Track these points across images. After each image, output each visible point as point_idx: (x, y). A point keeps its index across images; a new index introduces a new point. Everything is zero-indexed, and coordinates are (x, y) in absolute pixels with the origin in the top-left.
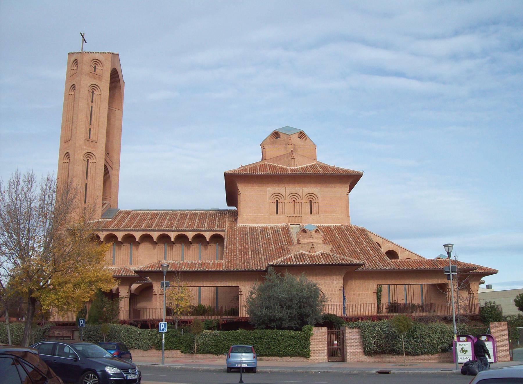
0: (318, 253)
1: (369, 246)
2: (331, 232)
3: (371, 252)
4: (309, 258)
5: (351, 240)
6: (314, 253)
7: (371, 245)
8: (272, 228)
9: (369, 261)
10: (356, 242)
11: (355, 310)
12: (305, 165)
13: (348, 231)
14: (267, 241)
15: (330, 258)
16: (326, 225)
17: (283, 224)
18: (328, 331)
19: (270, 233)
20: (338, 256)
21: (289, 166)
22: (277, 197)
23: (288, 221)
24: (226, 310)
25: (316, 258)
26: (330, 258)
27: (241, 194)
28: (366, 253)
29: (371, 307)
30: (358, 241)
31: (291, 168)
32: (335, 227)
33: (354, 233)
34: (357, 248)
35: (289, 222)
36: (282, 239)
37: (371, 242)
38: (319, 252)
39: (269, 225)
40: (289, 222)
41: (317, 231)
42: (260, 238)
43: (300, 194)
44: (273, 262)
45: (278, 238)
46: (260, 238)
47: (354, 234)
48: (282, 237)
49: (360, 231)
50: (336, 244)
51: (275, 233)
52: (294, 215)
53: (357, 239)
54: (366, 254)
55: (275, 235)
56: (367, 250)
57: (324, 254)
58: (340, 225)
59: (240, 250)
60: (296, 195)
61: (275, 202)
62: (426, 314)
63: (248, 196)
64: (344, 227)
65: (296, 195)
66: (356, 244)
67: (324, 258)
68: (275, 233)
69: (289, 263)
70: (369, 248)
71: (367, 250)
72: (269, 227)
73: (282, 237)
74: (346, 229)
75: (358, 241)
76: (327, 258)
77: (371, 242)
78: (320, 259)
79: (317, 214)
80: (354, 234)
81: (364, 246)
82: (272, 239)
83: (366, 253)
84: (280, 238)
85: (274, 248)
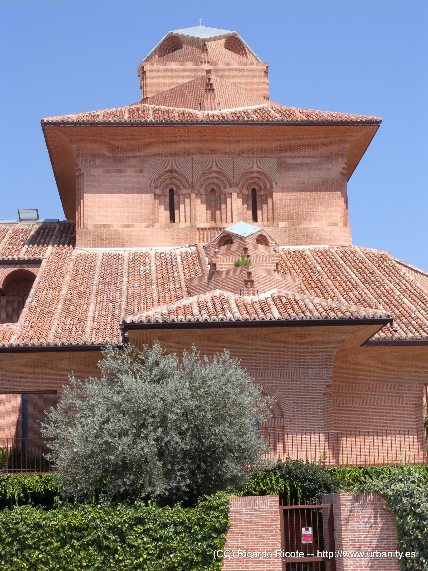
0: (262, 296)
1: (401, 289)
2: (303, 261)
3: (406, 301)
4: (238, 307)
5: (354, 276)
6: (254, 295)
7: (405, 288)
8: (158, 256)
9: (401, 320)
10: (367, 282)
11: (367, 451)
12: (241, 109)
13: (345, 259)
14: (142, 280)
15: (296, 306)
16: (292, 248)
17: (187, 245)
18: (289, 507)
19: (153, 264)
20: (317, 301)
21: (201, 106)
22: (172, 181)
23: (199, 240)
24: (337, 519)
25: (257, 306)
26: (296, 306)
27: (83, 174)
28: (393, 304)
29: (407, 444)
30: (372, 278)
31: (206, 112)
32: (313, 252)
33: (361, 263)
34: (368, 292)
35: (201, 241)
36: (179, 277)
37: (403, 281)
38: (268, 294)
39: (152, 251)
40: (201, 241)
41: (261, 239)
42: (125, 274)
43: (228, 172)
44: (138, 316)
45: (170, 274)
46: (125, 274)
47: (360, 265)
48: (181, 273)
49: (375, 258)
50: (315, 286)
51: (164, 265)
52: (213, 225)
53: (369, 275)
54: (393, 307)
55: (164, 269)
56: (396, 297)
57: (280, 297)
58: (327, 247)
59: (67, 302)
60: (217, 175)
61: (167, 193)
62: (344, 522)
63: (102, 179)
64: (336, 252)
65: (217, 175)
66: (367, 285)
67: (280, 305)
68: (164, 265)
69: (181, 317)
70: (398, 293)
71: (394, 298)
72: (153, 253)
73: (181, 273)
74: (341, 254)
75: (372, 278)
76: (288, 306)
77: (403, 281)
78: (270, 309)
79: (271, 221)
80: (360, 265)
81: (387, 288)
82: (154, 277)
83: (393, 304)
84: (176, 274)
85: (155, 295)
